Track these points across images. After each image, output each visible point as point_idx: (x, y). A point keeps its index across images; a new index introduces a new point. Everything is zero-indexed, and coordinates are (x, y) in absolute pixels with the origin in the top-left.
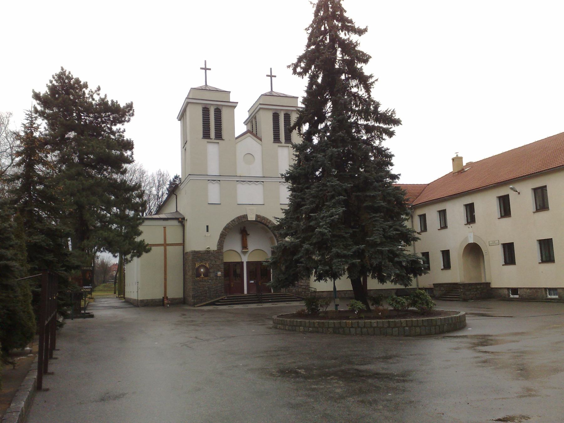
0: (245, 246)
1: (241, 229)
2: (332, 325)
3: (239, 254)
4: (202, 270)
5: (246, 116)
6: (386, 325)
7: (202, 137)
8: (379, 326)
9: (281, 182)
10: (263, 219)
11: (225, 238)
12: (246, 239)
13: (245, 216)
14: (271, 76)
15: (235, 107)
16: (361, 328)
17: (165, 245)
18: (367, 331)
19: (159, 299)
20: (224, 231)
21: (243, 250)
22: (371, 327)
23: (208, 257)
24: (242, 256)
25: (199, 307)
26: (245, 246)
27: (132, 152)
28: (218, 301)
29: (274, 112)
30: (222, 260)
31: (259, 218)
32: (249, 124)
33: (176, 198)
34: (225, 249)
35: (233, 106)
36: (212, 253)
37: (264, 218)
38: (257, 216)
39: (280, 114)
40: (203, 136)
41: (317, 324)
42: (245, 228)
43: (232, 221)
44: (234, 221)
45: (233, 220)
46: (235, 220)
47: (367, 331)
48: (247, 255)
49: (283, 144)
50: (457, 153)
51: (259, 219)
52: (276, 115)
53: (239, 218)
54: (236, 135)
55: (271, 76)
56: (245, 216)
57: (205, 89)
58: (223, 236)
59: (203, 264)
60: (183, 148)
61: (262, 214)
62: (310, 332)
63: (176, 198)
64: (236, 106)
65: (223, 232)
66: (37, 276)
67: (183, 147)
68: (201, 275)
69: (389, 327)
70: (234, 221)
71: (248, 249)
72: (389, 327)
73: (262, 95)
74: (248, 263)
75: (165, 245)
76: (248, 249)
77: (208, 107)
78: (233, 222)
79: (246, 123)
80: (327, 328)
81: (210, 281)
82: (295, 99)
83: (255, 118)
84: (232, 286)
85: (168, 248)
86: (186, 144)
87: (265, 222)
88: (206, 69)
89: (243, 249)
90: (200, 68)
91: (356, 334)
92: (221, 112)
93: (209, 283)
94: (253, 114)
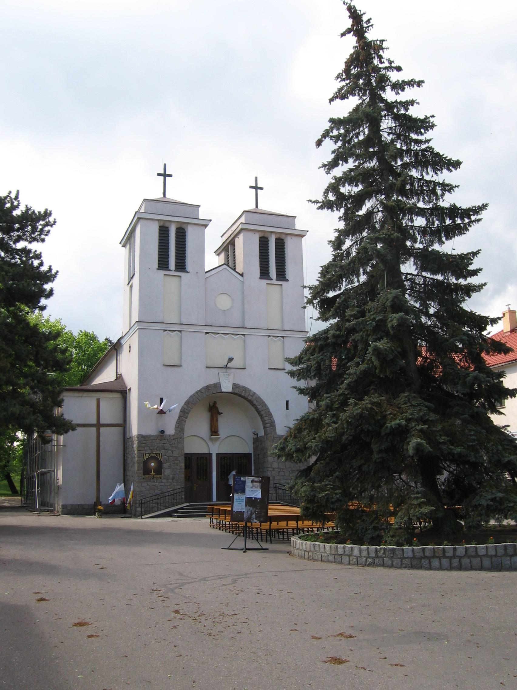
0: (214, 431)
1: (210, 405)
2: (410, 555)
3: (205, 441)
4: (153, 464)
5: (219, 242)
6: (501, 552)
7: (157, 268)
8: (489, 554)
9: (270, 336)
10: (243, 391)
11: (186, 418)
12: (217, 421)
13: (217, 385)
14: (256, 188)
15: (206, 226)
16: (460, 558)
17: (99, 425)
18: (471, 562)
19: (89, 505)
20: (186, 407)
21: (212, 437)
22: (477, 555)
23: (162, 444)
24: (210, 444)
25: (147, 519)
26: (214, 431)
27: (19, 201)
28: (176, 511)
29: (261, 236)
30: (183, 449)
31: (238, 389)
32: (223, 255)
33: (117, 360)
34: (187, 433)
35: (204, 225)
36: (167, 439)
37: (245, 389)
38: (235, 386)
39: (269, 239)
40: (158, 267)
41: (382, 552)
42: (215, 403)
43: (197, 392)
44: (201, 392)
45: (200, 391)
46: (203, 391)
47: (471, 562)
48: (218, 443)
49: (274, 281)
50: (508, 305)
51: (237, 391)
52: (263, 239)
53: (208, 388)
54: (206, 271)
55: (256, 188)
56: (217, 385)
57: (163, 201)
58: (184, 413)
59: (154, 455)
60: (128, 284)
61: (242, 383)
62: (368, 564)
63: (117, 360)
64: (208, 225)
65: (184, 408)
66: (35, 500)
67: (127, 283)
68: (151, 472)
69: (506, 555)
70: (201, 392)
71: (219, 435)
72: (506, 555)
73: (244, 211)
74: (218, 455)
75: (99, 425)
76: (219, 435)
77: (167, 225)
78: (199, 393)
79: (218, 252)
80: (400, 558)
81: (163, 481)
82: (290, 219)
83: (234, 245)
84: (195, 489)
85: (102, 429)
86: (132, 278)
87: (247, 394)
88: (165, 175)
89: (212, 435)
90: (156, 174)
91: (450, 568)
92: (185, 233)
93: (162, 484)
94: (230, 239)
